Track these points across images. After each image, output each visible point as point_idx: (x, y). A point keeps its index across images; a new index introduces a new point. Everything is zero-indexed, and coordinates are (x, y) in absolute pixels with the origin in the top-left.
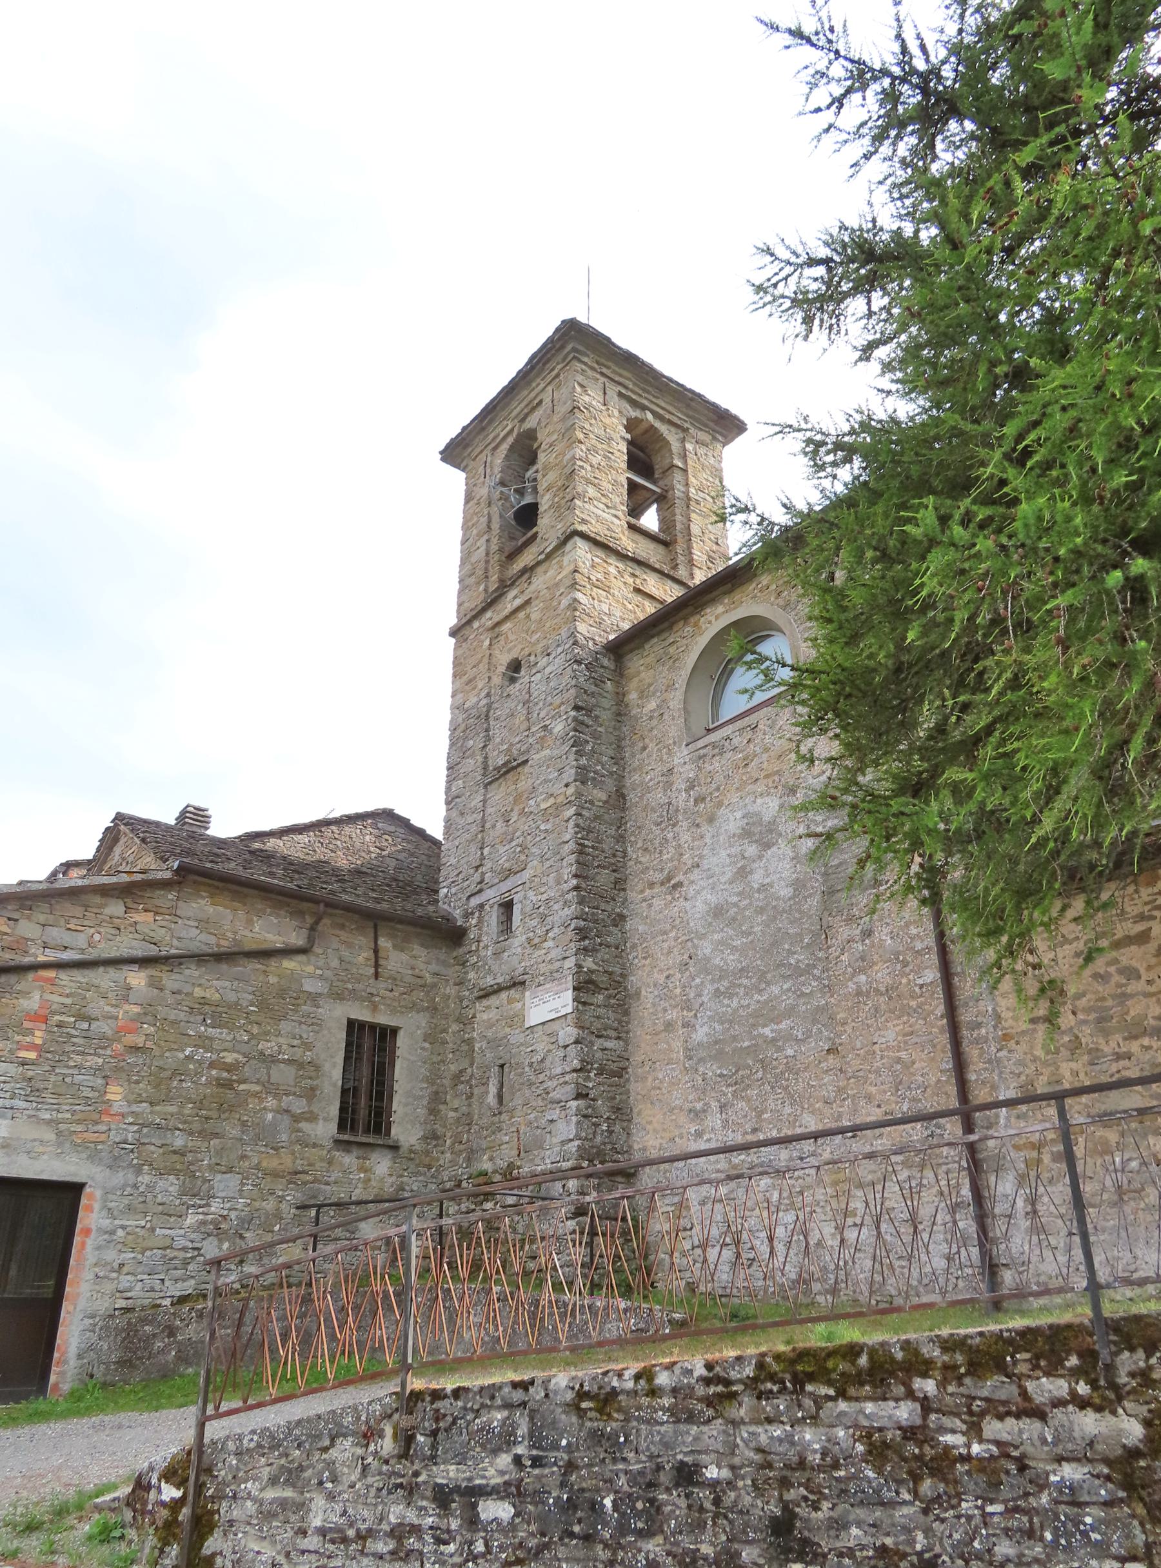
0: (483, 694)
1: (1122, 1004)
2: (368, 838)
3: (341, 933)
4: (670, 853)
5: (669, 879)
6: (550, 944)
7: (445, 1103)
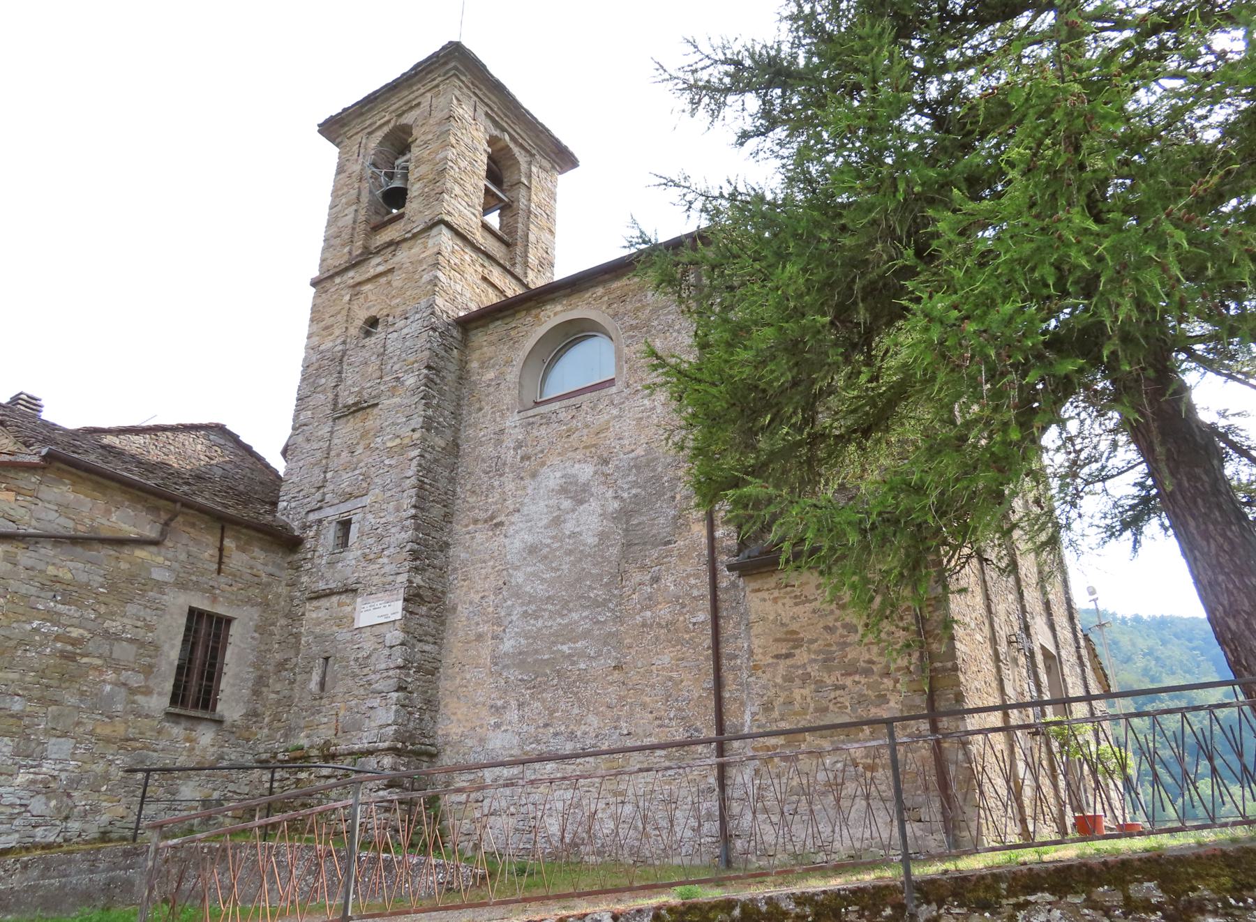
0: (339, 341)
1: (842, 649)
2: (199, 447)
3: (192, 530)
4: (495, 497)
5: (492, 518)
6: (385, 560)
7: (268, 686)
